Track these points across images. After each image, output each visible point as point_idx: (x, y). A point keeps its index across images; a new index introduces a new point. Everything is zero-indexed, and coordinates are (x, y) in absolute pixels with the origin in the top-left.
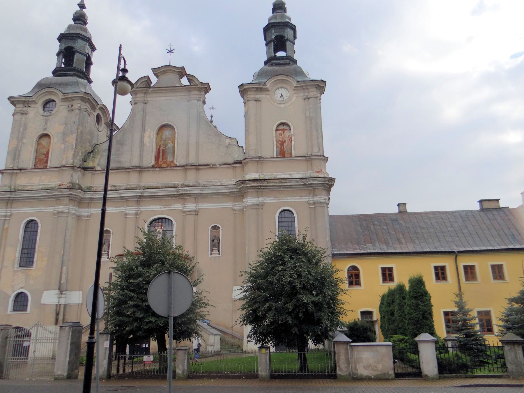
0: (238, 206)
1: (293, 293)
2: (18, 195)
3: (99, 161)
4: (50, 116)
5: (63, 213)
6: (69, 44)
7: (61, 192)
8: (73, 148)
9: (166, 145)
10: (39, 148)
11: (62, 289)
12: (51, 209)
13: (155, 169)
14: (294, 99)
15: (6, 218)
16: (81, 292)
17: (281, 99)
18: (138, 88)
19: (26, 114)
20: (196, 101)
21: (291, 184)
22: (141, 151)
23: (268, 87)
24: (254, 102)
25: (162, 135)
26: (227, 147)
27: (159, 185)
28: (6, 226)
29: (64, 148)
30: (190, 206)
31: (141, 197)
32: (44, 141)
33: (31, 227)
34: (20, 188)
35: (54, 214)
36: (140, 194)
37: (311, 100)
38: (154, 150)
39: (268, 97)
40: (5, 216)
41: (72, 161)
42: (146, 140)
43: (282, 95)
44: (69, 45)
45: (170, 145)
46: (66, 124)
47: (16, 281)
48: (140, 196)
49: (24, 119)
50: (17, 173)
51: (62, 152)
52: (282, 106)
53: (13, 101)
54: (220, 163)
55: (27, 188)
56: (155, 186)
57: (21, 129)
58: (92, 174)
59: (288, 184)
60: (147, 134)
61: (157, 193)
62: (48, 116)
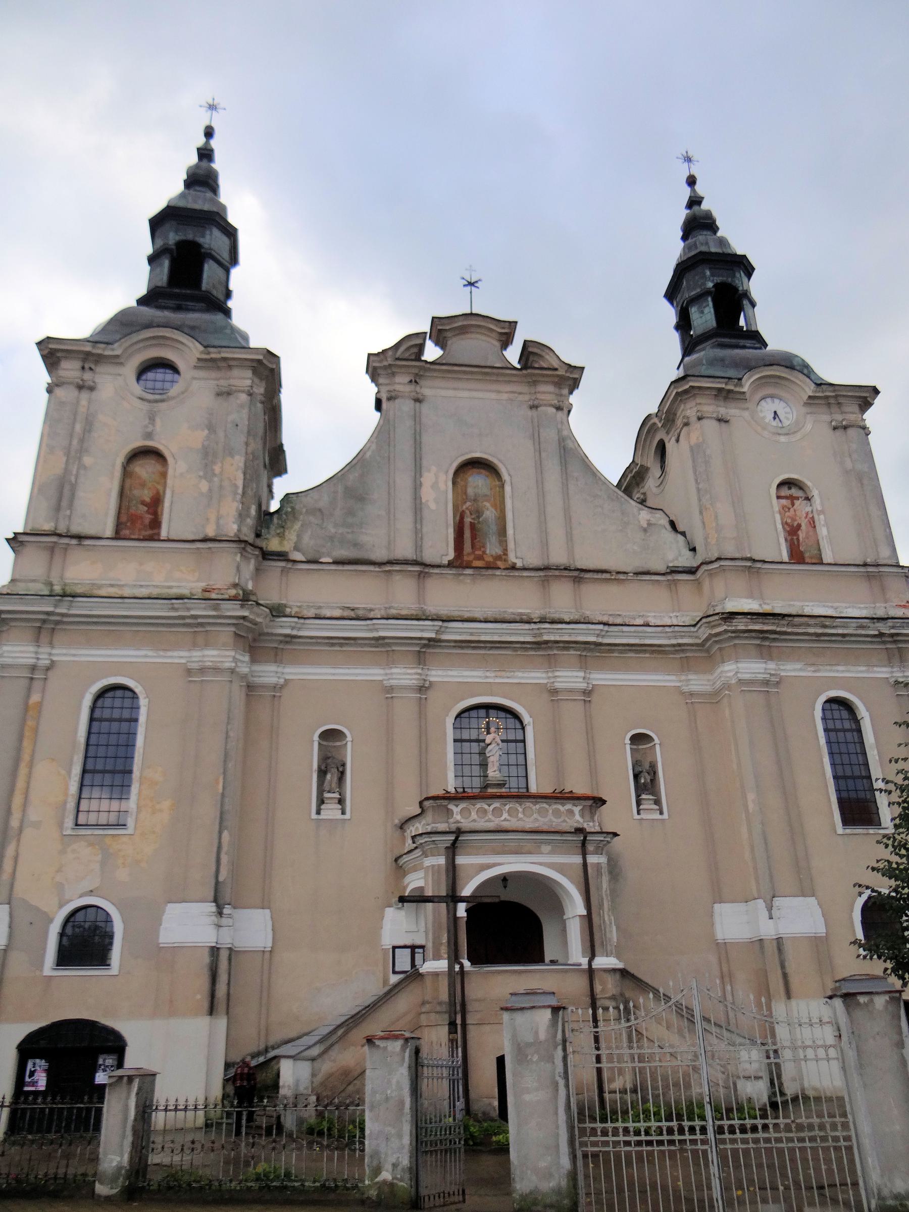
0: (697, 682)
1: (414, 976)
2: (80, 608)
3: (299, 536)
4: (162, 401)
5: (216, 670)
6: (190, 234)
7: (216, 608)
8: (236, 493)
9: (479, 513)
10: (127, 485)
11: (221, 902)
12: (179, 656)
13: (460, 571)
14: (809, 426)
15: (36, 674)
16: (267, 911)
17: (774, 423)
18: (398, 359)
19: (92, 389)
20: (554, 410)
21: (846, 632)
22: (416, 522)
23: (745, 389)
24: (715, 423)
25: (466, 487)
26: (645, 530)
27: (478, 615)
28: (35, 698)
29: (210, 490)
30: (570, 678)
31: (432, 643)
32: (145, 469)
33: (114, 707)
34: (79, 590)
35: (189, 672)
36: (433, 635)
37: (851, 431)
38: (451, 522)
39: (746, 414)
40: (33, 668)
41: (235, 527)
42: (428, 494)
43: (775, 412)
44: (190, 237)
45: (490, 513)
46: (211, 428)
47: (59, 876)
48: (430, 640)
49: (84, 402)
50: (66, 548)
51: (199, 500)
52: (783, 439)
53: (53, 352)
55: (103, 592)
56: (467, 615)
57: (78, 427)
58: (283, 570)
59: (840, 631)
60: (428, 479)
61: (479, 634)
62: (156, 401)
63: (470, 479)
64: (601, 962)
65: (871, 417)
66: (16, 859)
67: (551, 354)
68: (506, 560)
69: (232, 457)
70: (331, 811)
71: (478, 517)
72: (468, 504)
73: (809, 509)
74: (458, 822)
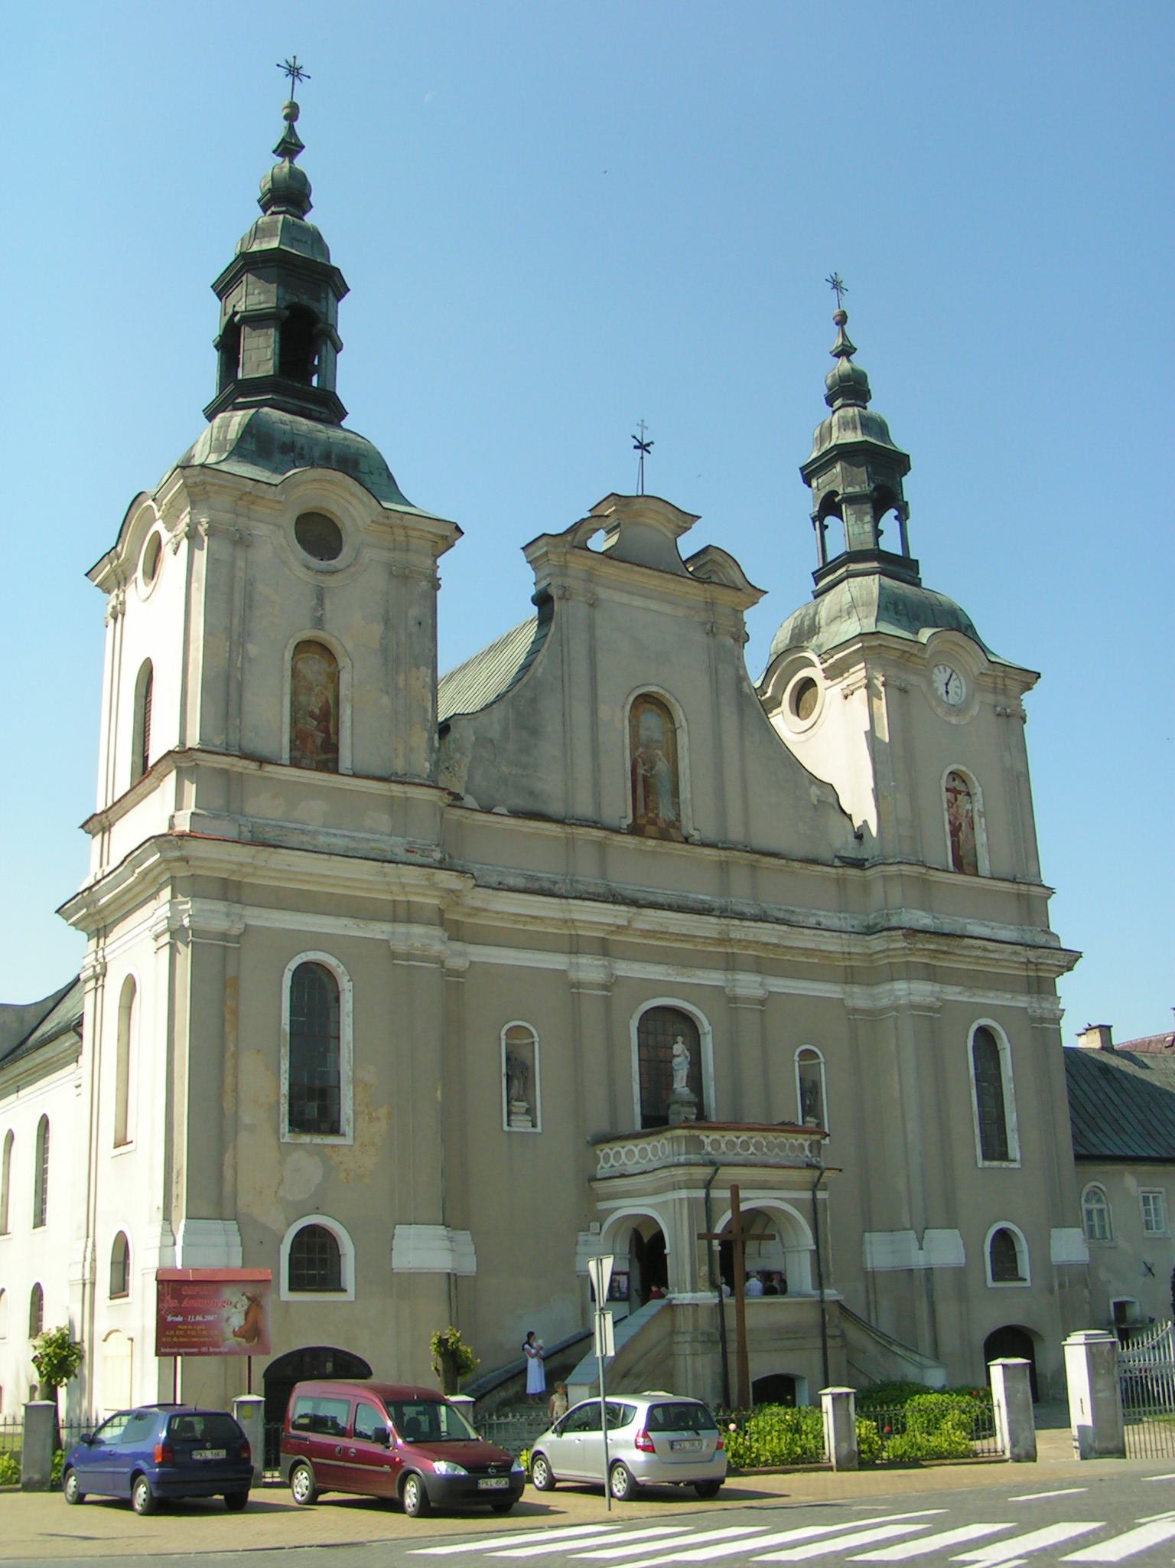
27: (661, 899)
30: (748, 985)
45: (662, 766)
48: (618, 927)
49: (240, 563)
54: (801, 854)
63: (642, 717)
64: (831, 1294)
65: (1028, 700)
66: (235, 1168)
67: (736, 568)
68: (679, 829)
69: (418, 668)
70: (521, 1125)
71: (652, 768)
72: (641, 750)
73: (969, 807)
74: (708, 1154)
